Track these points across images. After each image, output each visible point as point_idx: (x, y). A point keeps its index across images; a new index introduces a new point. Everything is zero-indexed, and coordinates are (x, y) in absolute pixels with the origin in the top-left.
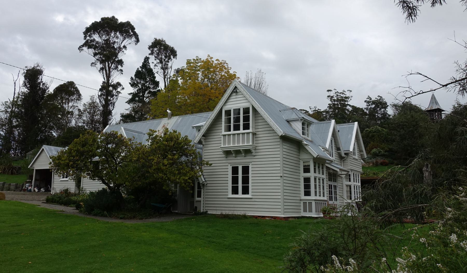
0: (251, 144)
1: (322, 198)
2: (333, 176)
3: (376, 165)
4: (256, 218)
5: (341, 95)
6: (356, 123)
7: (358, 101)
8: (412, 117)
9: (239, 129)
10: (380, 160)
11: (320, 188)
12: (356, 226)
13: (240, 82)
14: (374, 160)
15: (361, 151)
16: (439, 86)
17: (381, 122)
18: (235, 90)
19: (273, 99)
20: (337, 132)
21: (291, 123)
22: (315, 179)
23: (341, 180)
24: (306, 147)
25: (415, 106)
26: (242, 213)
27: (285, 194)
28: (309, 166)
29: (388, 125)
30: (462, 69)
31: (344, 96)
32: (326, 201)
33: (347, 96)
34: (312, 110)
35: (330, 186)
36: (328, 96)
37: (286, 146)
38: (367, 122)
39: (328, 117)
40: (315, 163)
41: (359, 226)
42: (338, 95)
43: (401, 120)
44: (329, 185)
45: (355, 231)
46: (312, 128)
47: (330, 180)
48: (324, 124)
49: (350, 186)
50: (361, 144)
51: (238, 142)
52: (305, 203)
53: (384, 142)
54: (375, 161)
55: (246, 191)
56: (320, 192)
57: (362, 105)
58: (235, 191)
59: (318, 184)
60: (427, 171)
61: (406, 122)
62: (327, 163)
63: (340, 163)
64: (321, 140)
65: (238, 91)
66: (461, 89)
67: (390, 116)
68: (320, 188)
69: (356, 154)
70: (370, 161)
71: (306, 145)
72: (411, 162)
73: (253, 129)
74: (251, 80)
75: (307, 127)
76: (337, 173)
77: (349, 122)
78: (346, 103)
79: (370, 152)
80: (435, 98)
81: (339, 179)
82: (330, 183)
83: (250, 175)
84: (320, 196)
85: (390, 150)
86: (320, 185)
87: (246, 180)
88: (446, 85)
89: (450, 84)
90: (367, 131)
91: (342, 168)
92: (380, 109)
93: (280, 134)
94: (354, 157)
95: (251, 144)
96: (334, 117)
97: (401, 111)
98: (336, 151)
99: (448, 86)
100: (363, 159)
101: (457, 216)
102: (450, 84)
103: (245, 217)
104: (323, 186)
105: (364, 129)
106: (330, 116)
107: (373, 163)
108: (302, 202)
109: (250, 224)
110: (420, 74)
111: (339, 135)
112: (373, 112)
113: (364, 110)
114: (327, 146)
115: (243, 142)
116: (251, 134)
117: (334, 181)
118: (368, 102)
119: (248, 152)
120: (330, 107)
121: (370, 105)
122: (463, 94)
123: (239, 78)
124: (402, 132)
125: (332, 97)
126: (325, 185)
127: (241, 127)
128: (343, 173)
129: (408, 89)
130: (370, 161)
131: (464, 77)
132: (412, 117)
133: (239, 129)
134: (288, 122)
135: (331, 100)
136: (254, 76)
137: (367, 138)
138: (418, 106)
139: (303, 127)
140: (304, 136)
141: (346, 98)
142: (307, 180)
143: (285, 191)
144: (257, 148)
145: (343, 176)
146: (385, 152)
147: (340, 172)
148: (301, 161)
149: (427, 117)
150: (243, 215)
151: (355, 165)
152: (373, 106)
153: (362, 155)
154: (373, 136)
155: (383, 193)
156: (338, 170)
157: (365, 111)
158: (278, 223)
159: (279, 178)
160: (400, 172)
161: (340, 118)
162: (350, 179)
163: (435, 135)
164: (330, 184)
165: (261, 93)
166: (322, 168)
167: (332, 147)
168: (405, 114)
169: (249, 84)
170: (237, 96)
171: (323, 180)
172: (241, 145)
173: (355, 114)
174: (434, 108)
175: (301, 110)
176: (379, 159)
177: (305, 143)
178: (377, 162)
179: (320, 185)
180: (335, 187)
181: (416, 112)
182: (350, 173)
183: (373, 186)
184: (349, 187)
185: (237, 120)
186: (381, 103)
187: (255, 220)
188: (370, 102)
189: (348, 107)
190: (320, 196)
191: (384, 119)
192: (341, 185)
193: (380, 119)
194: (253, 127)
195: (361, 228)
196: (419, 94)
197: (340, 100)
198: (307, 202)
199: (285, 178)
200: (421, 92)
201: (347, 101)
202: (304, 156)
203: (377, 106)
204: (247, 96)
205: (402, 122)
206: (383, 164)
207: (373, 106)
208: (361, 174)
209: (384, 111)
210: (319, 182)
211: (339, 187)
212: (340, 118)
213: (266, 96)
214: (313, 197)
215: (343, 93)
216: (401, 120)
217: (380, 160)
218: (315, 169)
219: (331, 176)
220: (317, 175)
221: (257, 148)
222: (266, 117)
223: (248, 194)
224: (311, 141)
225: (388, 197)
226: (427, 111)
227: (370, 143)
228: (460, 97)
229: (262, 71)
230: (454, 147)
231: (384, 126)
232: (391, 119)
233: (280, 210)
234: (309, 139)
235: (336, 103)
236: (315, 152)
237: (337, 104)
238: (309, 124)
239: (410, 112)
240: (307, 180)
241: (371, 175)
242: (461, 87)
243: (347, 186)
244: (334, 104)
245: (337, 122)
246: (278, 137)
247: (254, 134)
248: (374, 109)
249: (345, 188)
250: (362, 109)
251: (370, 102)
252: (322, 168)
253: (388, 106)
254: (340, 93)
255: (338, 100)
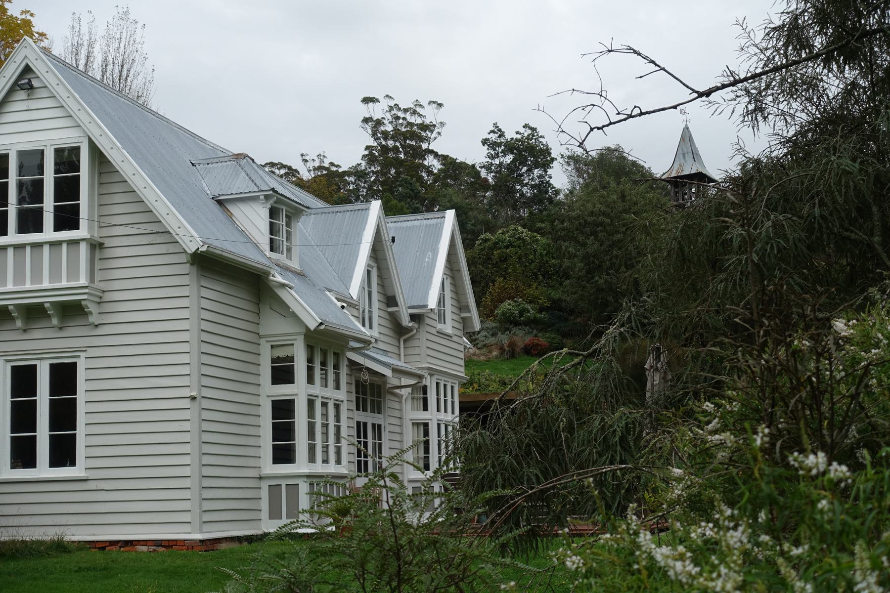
0: (83, 281)
1: (332, 468)
2: (371, 392)
3: (511, 353)
4: (103, 548)
5: (408, 116)
6: (451, 214)
7: (461, 142)
8: (623, 197)
9: (38, 227)
10: (522, 337)
11: (326, 434)
12: (404, 541)
13: (46, 51)
14: (504, 339)
15: (462, 307)
16: (686, 95)
17: (531, 213)
18: (26, 81)
19: (167, 121)
20: (389, 243)
21: (232, 208)
22: (311, 403)
23: (397, 406)
24: (283, 294)
25: (634, 163)
26: (49, 535)
27: (206, 460)
28: (291, 359)
29: (552, 222)
30: (756, 46)
31: (419, 121)
32: (343, 477)
33: (427, 122)
34: (311, 165)
35: (361, 429)
36: (366, 120)
37: (214, 293)
38: (487, 211)
39: (364, 192)
40: (310, 348)
41: (411, 541)
42: (398, 118)
43: (589, 205)
44: (358, 423)
45: (398, 559)
46: (304, 227)
47: (361, 405)
48: (344, 214)
49: (426, 425)
50: (463, 286)
51: (37, 275)
52: (274, 490)
53: (537, 278)
54: (506, 343)
55: (63, 453)
56: (326, 449)
57: (473, 154)
58: (23, 454)
59: (318, 420)
60: (657, 369)
61: (604, 214)
62: (353, 349)
63: (395, 350)
64: (334, 271)
65: (35, 83)
66: (751, 107)
67: (557, 192)
68: (326, 434)
69: (449, 316)
70: (492, 340)
71: (283, 286)
72: (599, 334)
73: (90, 228)
74: (90, 45)
75: (288, 225)
76: (385, 383)
77: (430, 210)
78: (424, 146)
79: (492, 311)
80: (691, 139)
81: (390, 403)
82: (361, 417)
83: (81, 397)
84: (326, 461)
85: (555, 306)
86: (325, 426)
87: (64, 415)
88: (708, 93)
89: (717, 89)
90: (486, 240)
91: (400, 364)
92: (530, 170)
93: (191, 248)
94: (440, 326)
95: (83, 281)
96: (384, 191)
97: (592, 177)
98: (383, 306)
99: (714, 96)
100: (472, 336)
101: (695, 490)
102: (717, 89)
103: (60, 547)
104: (338, 429)
105: (476, 235)
106: (370, 188)
107: (502, 349)
108: (265, 485)
109: (80, 570)
110: (635, 52)
111: (394, 253)
112: (507, 180)
113: (478, 173)
114: (354, 290)
115: (55, 274)
116: (83, 248)
117: (373, 411)
118: (493, 145)
119: (71, 311)
120: (370, 158)
121: (497, 156)
122: (755, 126)
123: (42, 35)
124: (592, 246)
125: (379, 123)
126: (344, 423)
127: (48, 219)
128: (405, 381)
129: (596, 100)
130: (492, 340)
131: (759, 71)
132: (623, 197)
133: (38, 227)
134: (220, 203)
135: (374, 134)
136: (100, 31)
137: (485, 265)
138: (642, 163)
139: (271, 224)
140: (274, 255)
141: (424, 127)
142: (283, 409)
143: (207, 449)
144: (107, 297)
145: (405, 392)
146: (540, 311)
147: (393, 381)
148: (262, 341)
149: (664, 200)
150: (53, 542)
151: (444, 355)
152: (509, 159)
153: (465, 322)
154: (504, 259)
155: (514, 439)
156: (388, 372)
157: (483, 173)
158: (179, 562)
159: (186, 403)
160: (565, 371)
161: (402, 198)
162: (425, 401)
163: (669, 252)
164: (362, 420)
165: (126, 97)
166: (336, 367)
167: (370, 294)
168: (604, 188)
169: (82, 62)
170: (33, 104)
171: (337, 407)
172: (46, 284)
173: (450, 185)
174: (686, 172)
175: (272, 165)
176: (521, 333)
177: (279, 279)
178: (512, 345)
179: (325, 426)
180: (378, 429)
181: (635, 182)
182: (426, 382)
183: (485, 418)
184: (421, 428)
185: (32, 192)
186: (531, 149)
187: (99, 557)
188: (499, 145)
189: (430, 161)
190: (326, 461)
191: (541, 202)
192: (396, 421)
193: (528, 202)
194: (90, 220)
195: (420, 550)
196: (630, 116)
197: (406, 136)
198: (284, 483)
199: (206, 404)
200: (637, 111)
201: (427, 139)
202: (274, 326)
203: (520, 160)
204: (70, 102)
205: (592, 214)
206: (532, 351)
207: (509, 159)
208: (463, 385)
209: (540, 176)
210: (325, 415)
211: (389, 428)
212: (402, 198)
213: (144, 107)
214: (301, 466)
215: (415, 112)
216: (589, 206)
217: (522, 337)
218: (310, 370)
219: (364, 393)
220: (317, 389)
221: (107, 297)
222: (141, 187)
223: (73, 463)
224: (301, 275)
225: (528, 453)
226: (669, 181)
227: (494, 282)
228: (747, 131)
229: (132, 17)
230: (721, 287)
231: (539, 225)
232: (560, 203)
233: (186, 517)
234: (295, 264)
235: (390, 143)
236: (310, 309)
237: (395, 149)
238: (295, 212)
239: (619, 183)
240: (283, 409)
241: (494, 387)
242: (750, 102)
243: (416, 424)
244: (385, 149)
245: (389, 210)
246: (183, 258)
247: (96, 246)
248: (512, 168)
249: (410, 436)
250: (473, 166)
251: (499, 145)
252: (336, 367)
253: (553, 160)
254: (406, 110)
255: (397, 135)
